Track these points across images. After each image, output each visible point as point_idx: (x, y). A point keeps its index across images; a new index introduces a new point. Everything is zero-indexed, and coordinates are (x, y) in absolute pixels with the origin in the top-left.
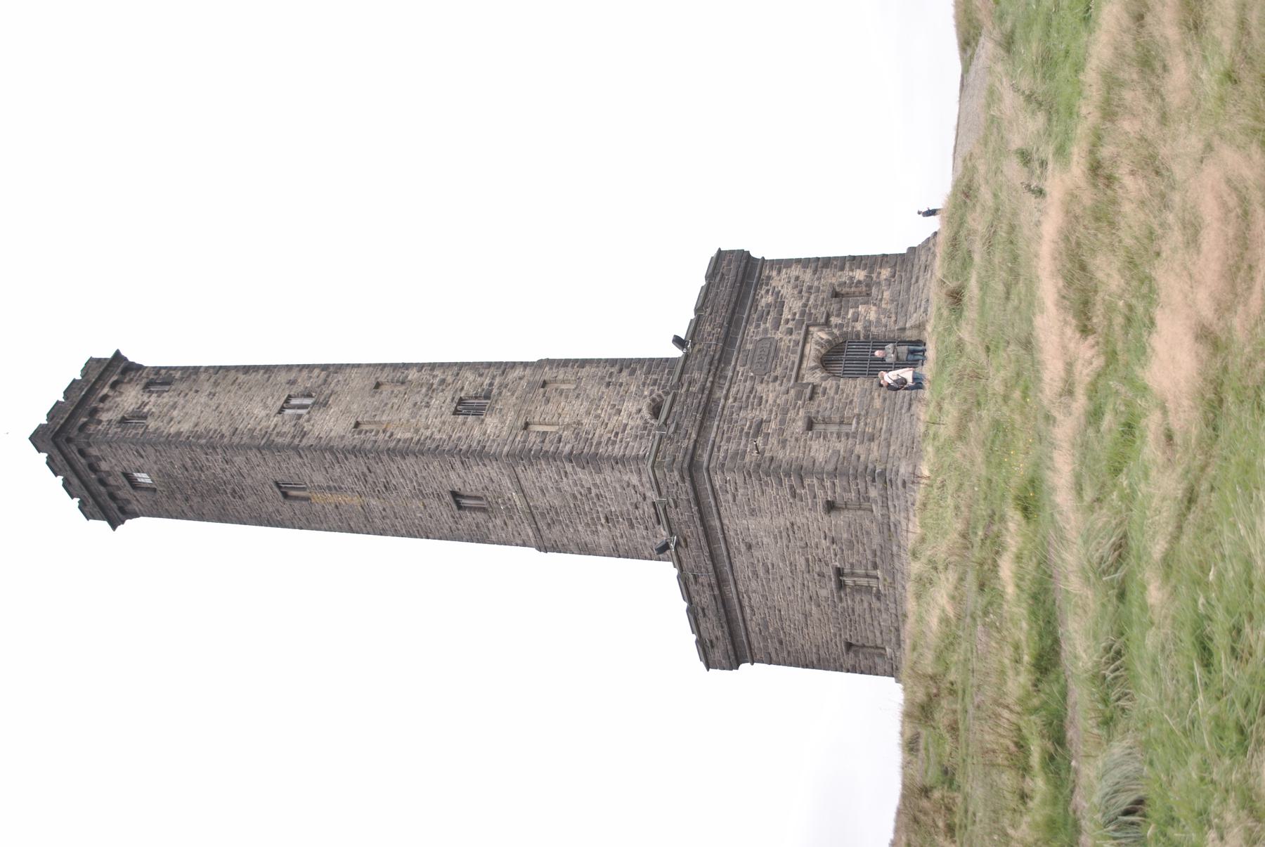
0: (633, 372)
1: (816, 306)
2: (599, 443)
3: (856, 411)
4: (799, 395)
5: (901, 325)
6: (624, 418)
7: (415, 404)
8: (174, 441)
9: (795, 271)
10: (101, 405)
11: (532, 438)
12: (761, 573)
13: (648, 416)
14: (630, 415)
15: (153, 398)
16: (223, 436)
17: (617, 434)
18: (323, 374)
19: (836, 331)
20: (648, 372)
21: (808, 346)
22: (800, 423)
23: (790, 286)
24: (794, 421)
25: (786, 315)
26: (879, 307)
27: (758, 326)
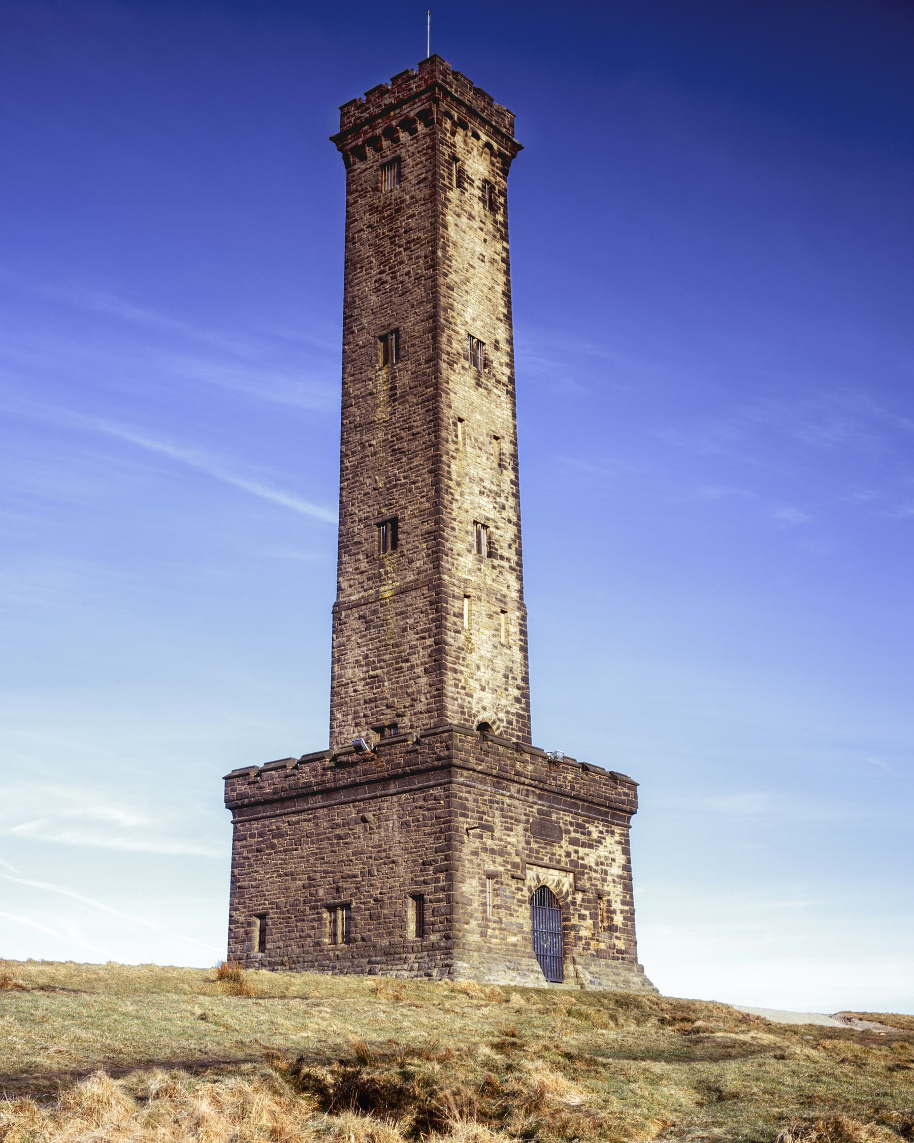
0: (518, 700)
1: (590, 879)
2: (455, 671)
3: (504, 920)
4: (515, 865)
5: (578, 959)
6: (478, 694)
7: (482, 480)
8: (436, 224)
9: (621, 859)
10: (470, 134)
11: (457, 604)
12: (338, 831)
13: (480, 718)
14: (481, 699)
15: (478, 193)
16: (446, 275)
17: (464, 688)
18: (505, 379)
19: (570, 898)
20: (519, 715)
21: (556, 872)
22: (492, 868)
23: (607, 854)
24: (494, 862)
25: (582, 851)
26: (592, 939)
27: (571, 824)
